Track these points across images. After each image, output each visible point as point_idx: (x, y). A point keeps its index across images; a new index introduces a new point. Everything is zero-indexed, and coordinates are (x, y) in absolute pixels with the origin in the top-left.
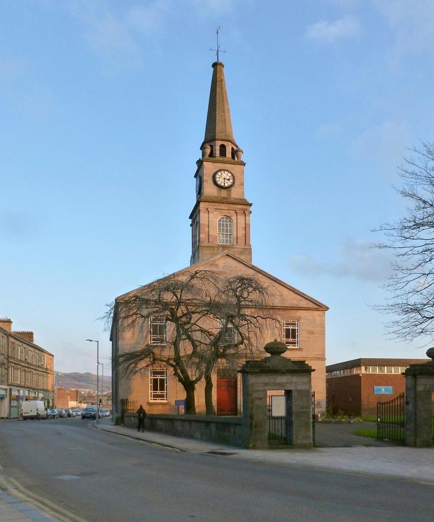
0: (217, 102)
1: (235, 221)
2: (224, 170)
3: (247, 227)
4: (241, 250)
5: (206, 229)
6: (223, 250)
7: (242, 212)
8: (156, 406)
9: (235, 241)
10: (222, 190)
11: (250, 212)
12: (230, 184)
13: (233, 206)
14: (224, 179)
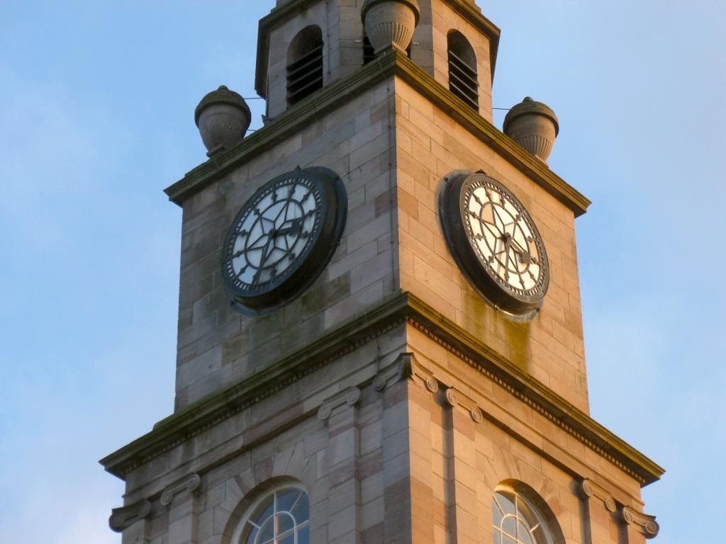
14: (505, 238)
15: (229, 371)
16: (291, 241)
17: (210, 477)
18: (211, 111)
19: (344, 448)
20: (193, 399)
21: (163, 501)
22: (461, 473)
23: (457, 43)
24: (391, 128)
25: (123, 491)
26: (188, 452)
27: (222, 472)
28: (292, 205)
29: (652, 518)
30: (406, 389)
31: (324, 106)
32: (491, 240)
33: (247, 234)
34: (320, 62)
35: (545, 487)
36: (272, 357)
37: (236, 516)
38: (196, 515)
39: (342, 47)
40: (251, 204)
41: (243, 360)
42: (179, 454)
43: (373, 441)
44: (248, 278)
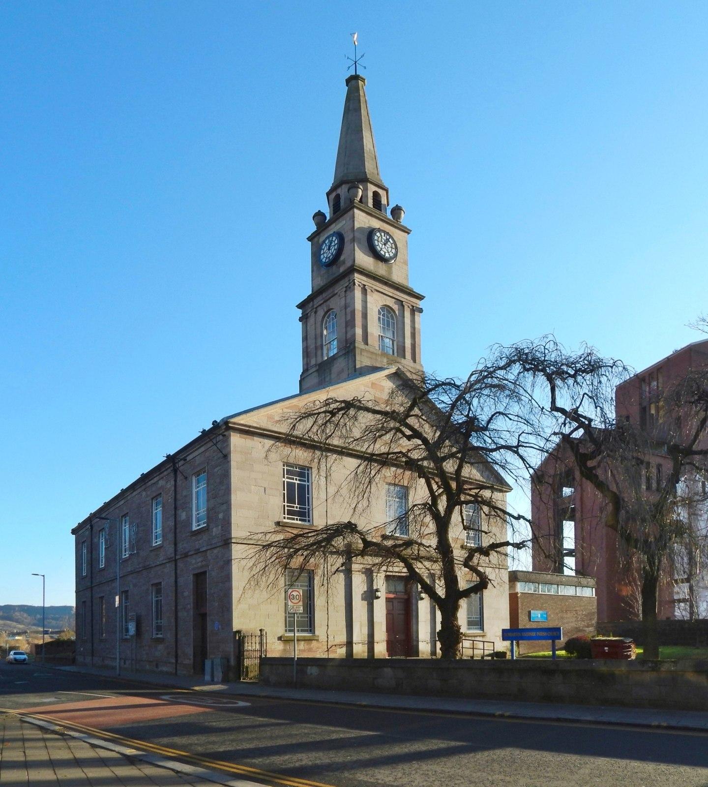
15: (321, 282)
18: (316, 217)
19: (343, 302)
20: (315, 289)
21: (309, 315)
24: (354, 221)
25: (301, 312)
26: (313, 302)
30: (354, 287)
31: (384, 628)
32: (380, 245)
34: (340, 204)
38: (315, 316)
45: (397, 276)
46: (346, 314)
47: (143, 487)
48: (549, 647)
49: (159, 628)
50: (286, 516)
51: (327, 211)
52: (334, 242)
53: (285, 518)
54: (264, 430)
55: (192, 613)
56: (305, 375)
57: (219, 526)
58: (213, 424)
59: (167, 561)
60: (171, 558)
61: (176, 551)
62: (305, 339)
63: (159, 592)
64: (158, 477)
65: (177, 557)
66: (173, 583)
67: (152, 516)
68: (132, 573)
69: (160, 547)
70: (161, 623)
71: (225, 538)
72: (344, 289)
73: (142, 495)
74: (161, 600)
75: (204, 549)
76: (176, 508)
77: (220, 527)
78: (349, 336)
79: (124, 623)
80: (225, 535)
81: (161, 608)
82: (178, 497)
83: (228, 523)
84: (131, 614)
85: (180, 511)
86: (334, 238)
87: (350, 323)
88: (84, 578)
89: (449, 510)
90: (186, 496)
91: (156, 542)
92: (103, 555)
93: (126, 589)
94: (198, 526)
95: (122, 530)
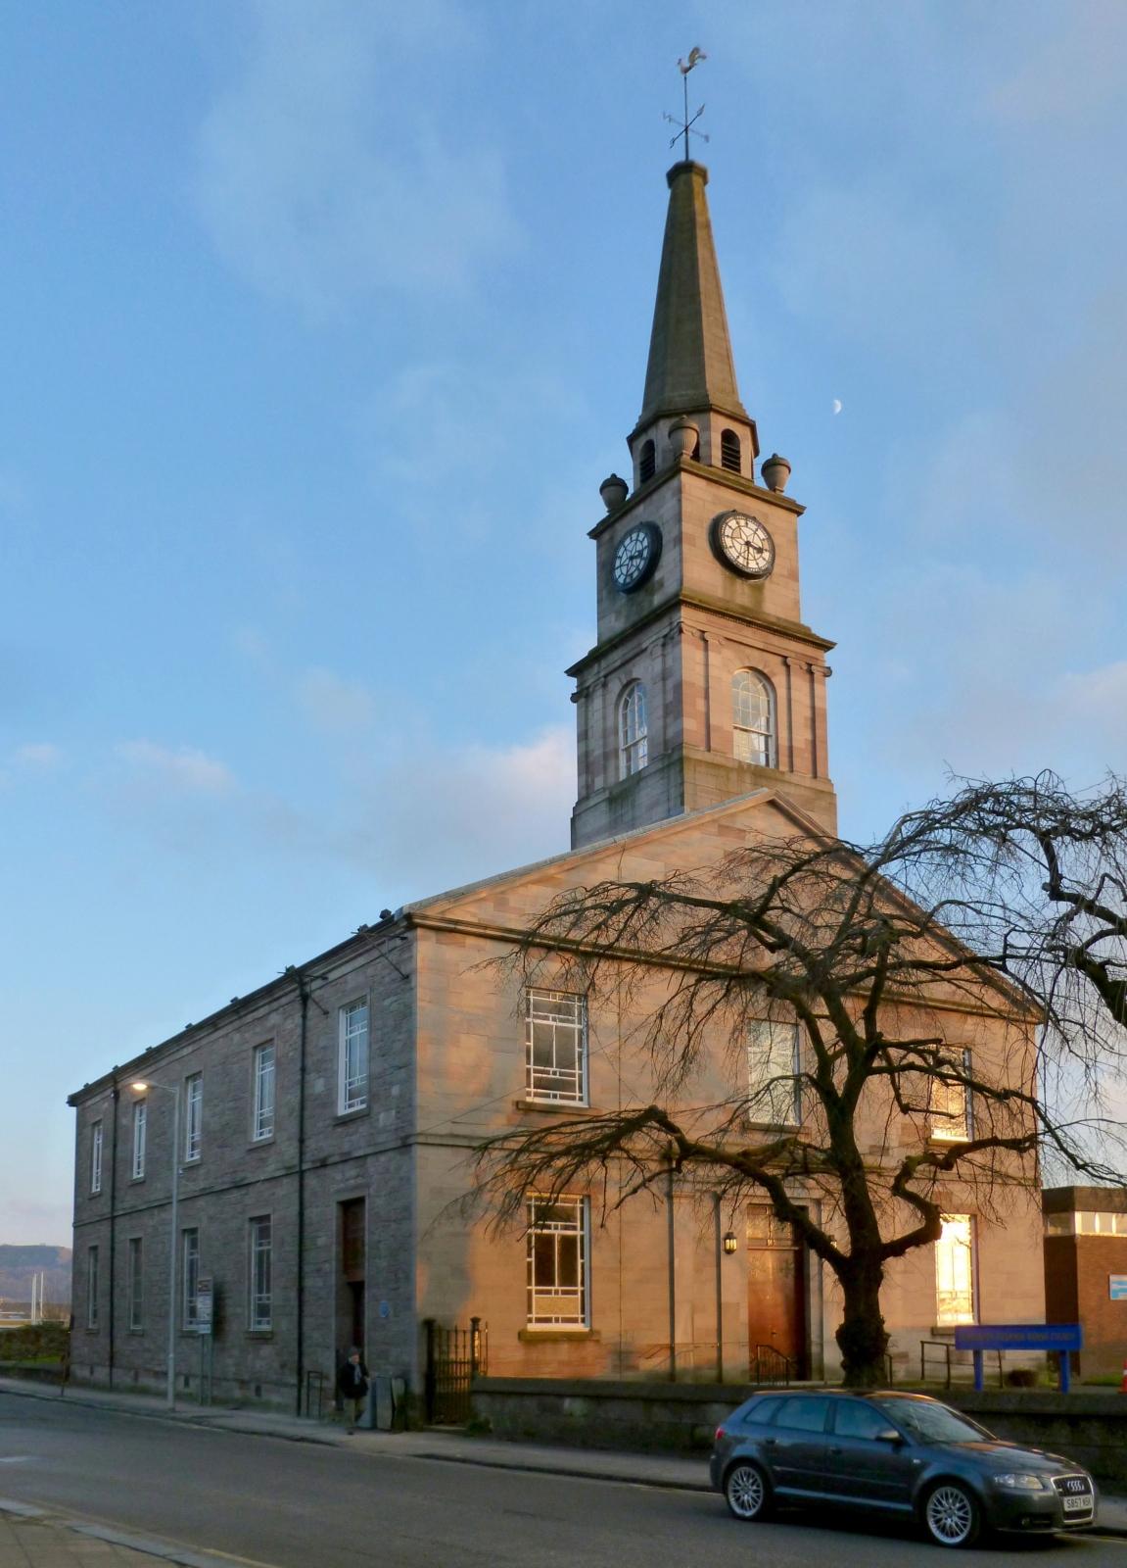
0: (702, 289)
1: (782, 692)
2: (747, 517)
3: (815, 719)
4: (807, 793)
5: (700, 704)
6: (756, 785)
7: (805, 667)
8: (549, 1348)
9: (784, 759)
10: (739, 582)
11: (828, 672)
12: (762, 564)
13: (777, 642)
14: (748, 544)
15: (618, 625)
16: (638, 561)
17: (609, 678)
19: (658, 666)
20: (605, 638)
21: (591, 689)
22: (713, 672)
23: (729, 437)
24: (680, 501)
26: (600, 665)
27: (613, 675)
28: (638, 543)
29: (829, 668)
32: (738, 546)
33: (621, 558)
34: (654, 461)
35: (765, 666)
36: (634, 618)
37: (620, 695)
38: (604, 695)
39: (664, 451)
40: (622, 542)
41: (623, 620)
42: (596, 668)
43: (669, 662)
44: (621, 580)
45: (774, 607)
46: (664, 692)
47: (237, 1024)
48: (294, 1263)
49: (263, 1311)
50: (532, 1090)
51: (628, 472)
52: (642, 542)
53: (529, 1094)
54: (486, 928)
55: (333, 1280)
56: (584, 806)
57: (392, 1109)
58: (381, 917)
59: (283, 1172)
60: (290, 1168)
61: (302, 1153)
62: (583, 736)
63: (264, 1234)
64: (267, 1007)
65: (305, 1167)
66: (295, 1219)
67: (253, 1080)
68: (206, 1193)
69: (268, 1146)
70: (268, 1298)
71: (403, 1134)
72: (661, 641)
73: (232, 1039)
74: (269, 1251)
75: (361, 1153)
76: (303, 1070)
77: (394, 1112)
78: (671, 732)
79: (185, 1294)
80: (403, 1127)
81: (268, 1268)
82: (309, 1048)
83: (410, 1106)
84: (203, 1277)
85: (312, 1075)
86: (642, 535)
87: (673, 709)
88: (93, 1198)
89: (855, 1085)
90: (325, 1048)
91: (261, 1134)
92: (143, 1153)
93: (193, 1225)
94: (350, 1106)
95: (186, 1106)
